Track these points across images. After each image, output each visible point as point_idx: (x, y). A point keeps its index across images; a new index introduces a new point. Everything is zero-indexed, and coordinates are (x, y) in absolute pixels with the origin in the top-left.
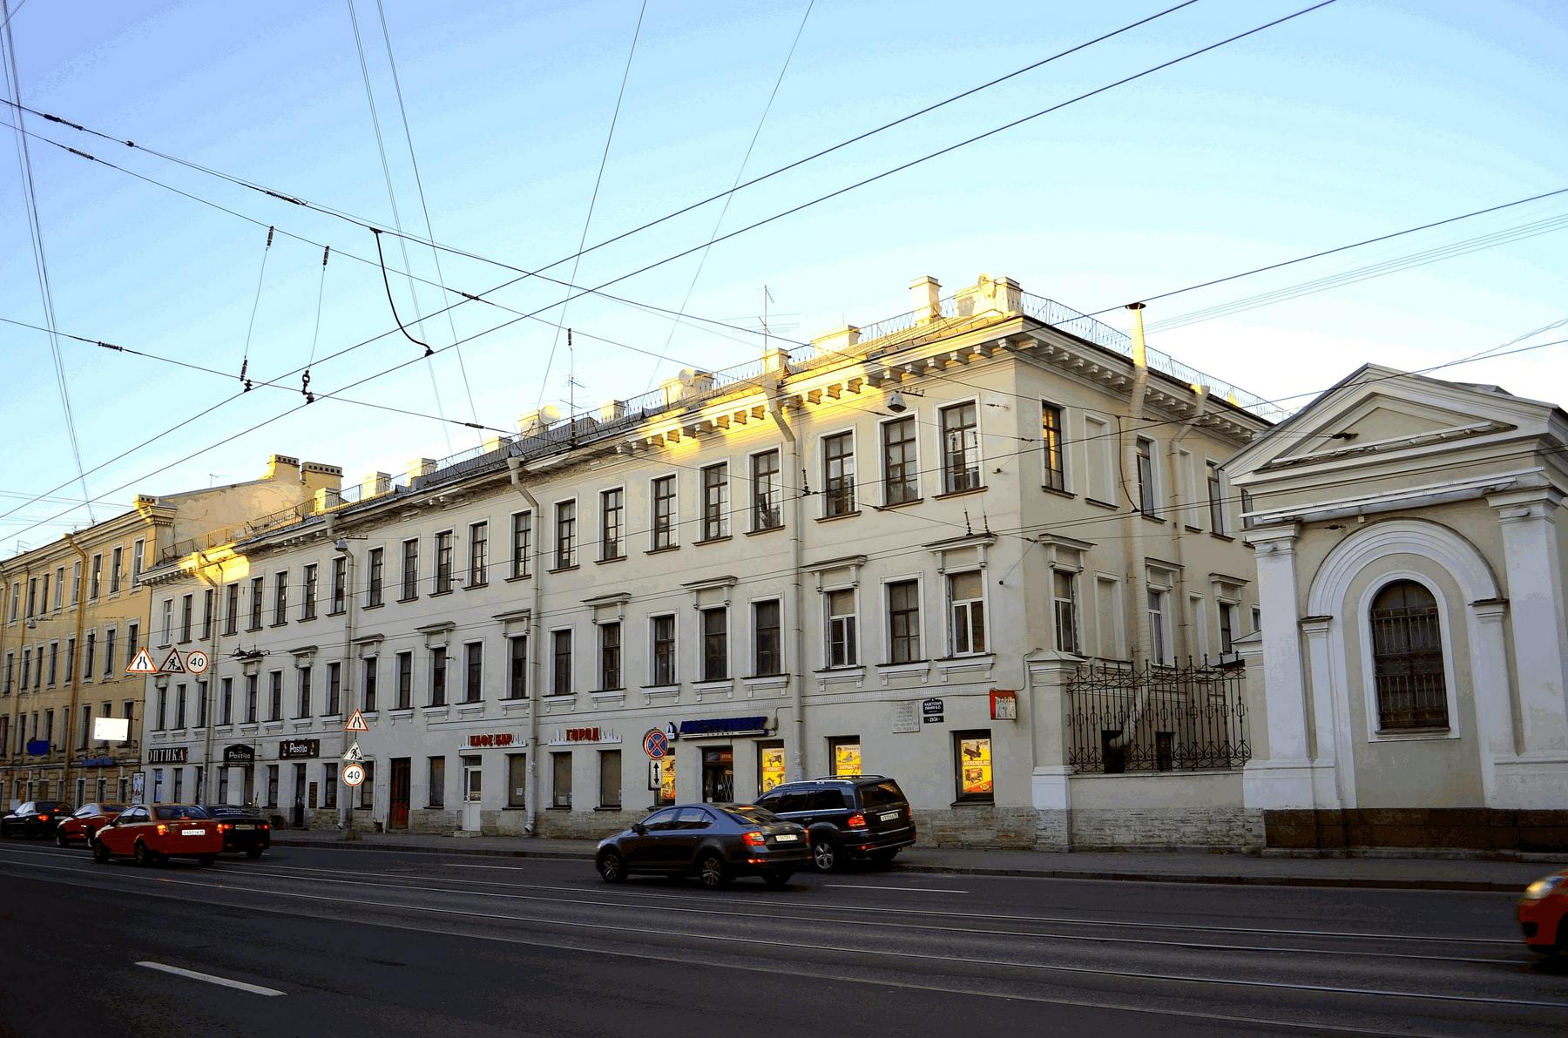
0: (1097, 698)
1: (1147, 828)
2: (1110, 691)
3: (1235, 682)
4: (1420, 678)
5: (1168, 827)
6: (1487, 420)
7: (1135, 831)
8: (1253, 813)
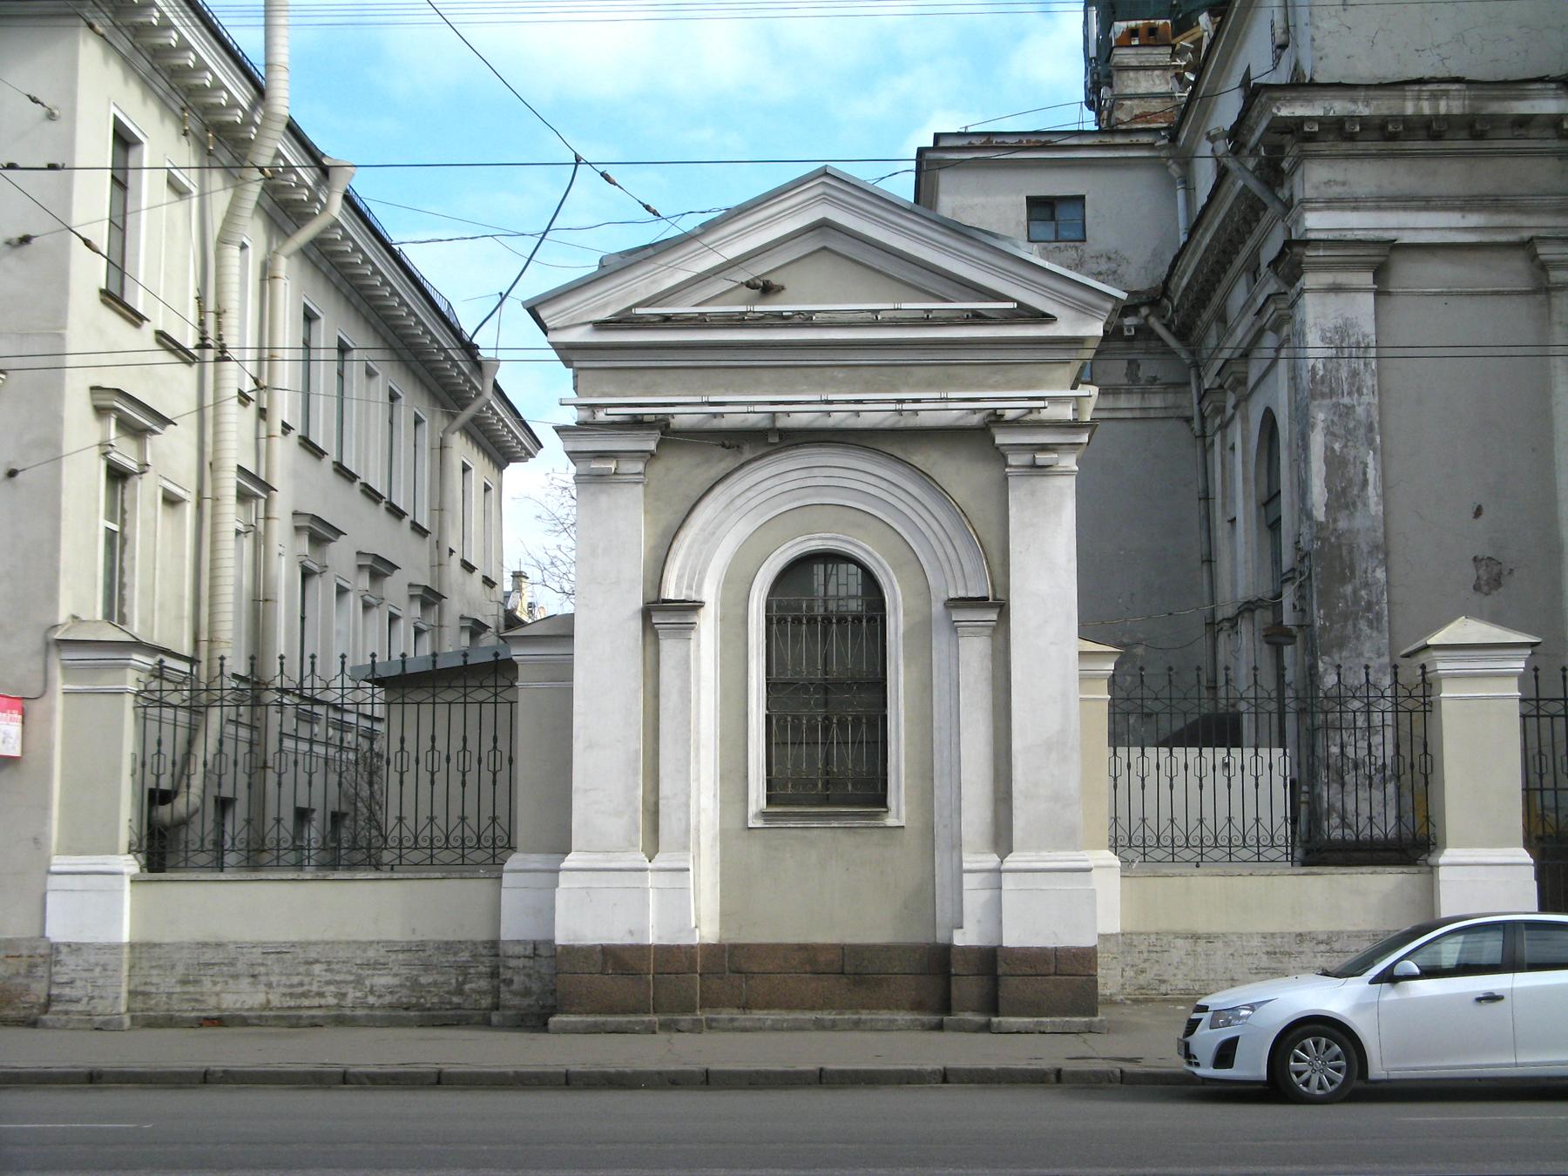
0: (1546, 735)
1: (296, 980)
2: (168, 713)
3: (488, 710)
4: (842, 725)
5: (338, 978)
6: (1013, 300)
7: (269, 985)
8: (518, 950)
